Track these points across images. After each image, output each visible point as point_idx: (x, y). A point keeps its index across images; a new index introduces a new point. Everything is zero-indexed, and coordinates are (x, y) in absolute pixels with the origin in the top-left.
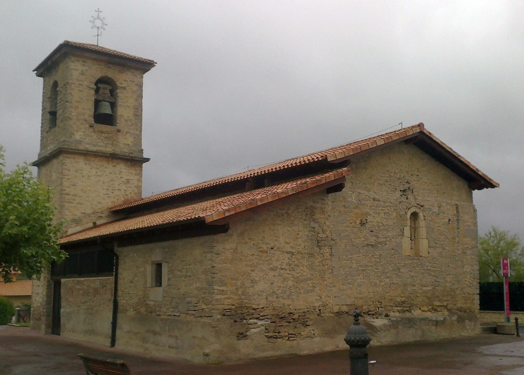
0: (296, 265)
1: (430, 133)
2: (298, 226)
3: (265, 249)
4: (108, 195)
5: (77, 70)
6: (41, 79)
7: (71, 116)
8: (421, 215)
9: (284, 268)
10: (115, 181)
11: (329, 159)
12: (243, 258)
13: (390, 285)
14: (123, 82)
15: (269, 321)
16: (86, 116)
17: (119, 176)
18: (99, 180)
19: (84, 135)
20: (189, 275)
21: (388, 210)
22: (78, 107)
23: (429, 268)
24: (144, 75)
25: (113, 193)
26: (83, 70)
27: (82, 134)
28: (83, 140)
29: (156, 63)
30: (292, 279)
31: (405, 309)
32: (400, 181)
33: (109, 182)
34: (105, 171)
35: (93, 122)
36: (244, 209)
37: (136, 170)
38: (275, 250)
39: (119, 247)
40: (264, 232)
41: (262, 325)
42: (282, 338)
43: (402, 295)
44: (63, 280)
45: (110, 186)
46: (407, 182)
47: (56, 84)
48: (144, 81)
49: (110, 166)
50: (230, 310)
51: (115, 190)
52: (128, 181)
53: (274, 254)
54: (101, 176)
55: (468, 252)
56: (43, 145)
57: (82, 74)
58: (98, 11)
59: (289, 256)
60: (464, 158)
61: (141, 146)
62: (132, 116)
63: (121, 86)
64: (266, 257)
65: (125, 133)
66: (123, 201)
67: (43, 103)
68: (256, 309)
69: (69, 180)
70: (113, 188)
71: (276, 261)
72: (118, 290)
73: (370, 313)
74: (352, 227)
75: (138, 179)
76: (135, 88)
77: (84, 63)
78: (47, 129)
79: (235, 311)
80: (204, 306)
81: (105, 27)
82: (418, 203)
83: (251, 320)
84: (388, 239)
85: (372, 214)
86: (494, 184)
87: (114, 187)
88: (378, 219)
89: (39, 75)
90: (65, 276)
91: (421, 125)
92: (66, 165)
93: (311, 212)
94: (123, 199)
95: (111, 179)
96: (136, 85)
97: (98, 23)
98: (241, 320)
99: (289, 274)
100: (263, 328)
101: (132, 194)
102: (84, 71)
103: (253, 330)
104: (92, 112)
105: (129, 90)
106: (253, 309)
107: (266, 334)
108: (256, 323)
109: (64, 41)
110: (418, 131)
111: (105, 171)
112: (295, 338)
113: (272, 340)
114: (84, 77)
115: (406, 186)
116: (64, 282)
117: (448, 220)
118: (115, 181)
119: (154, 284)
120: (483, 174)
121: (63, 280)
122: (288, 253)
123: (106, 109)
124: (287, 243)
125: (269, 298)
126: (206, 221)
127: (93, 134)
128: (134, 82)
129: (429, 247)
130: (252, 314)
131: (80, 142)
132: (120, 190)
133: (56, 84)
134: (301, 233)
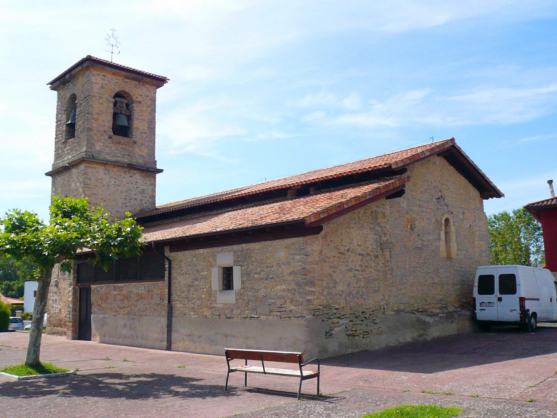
0: (366, 266)
1: (459, 147)
2: (366, 230)
3: (343, 251)
4: (126, 204)
5: (98, 83)
6: (55, 93)
7: (92, 128)
8: (451, 220)
9: (357, 269)
10: (132, 190)
11: (393, 167)
12: (326, 259)
13: (433, 284)
14: (138, 96)
15: (348, 320)
16: (106, 128)
17: (135, 186)
18: (118, 190)
19: (103, 146)
20: (271, 277)
21: (429, 215)
22: (98, 119)
23: (458, 268)
24: (157, 90)
25: (130, 202)
26: (102, 84)
27: (102, 144)
28: (102, 151)
29: (169, 80)
30: (364, 280)
31: (443, 306)
32: (435, 189)
33: (126, 192)
34: (122, 181)
35: (112, 134)
36: (334, 212)
37: (151, 181)
38: (351, 252)
39: (170, 252)
40: (342, 234)
41: (343, 324)
42: (358, 336)
43: (441, 293)
44: (93, 287)
45: (127, 196)
46: (440, 191)
47: (73, 97)
48: (157, 97)
49: (127, 176)
50: (318, 311)
51: (131, 199)
52: (143, 191)
53: (350, 256)
54: (119, 186)
55: (483, 255)
56: (58, 156)
57: (102, 87)
58: (113, 30)
59: (361, 257)
60: (481, 171)
61: (155, 158)
62: (146, 128)
63: (137, 100)
64: (344, 259)
65: (140, 145)
66: (139, 210)
67: (57, 115)
68: (338, 308)
69: (90, 189)
70: (130, 198)
71: (351, 263)
72: (173, 294)
73: (419, 310)
74: (406, 231)
75: (152, 189)
76: (149, 103)
77: (104, 78)
78: (63, 140)
79: (323, 311)
80: (292, 307)
81: (118, 45)
82: (449, 210)
83: (335, 320)
84: (430, 242)
85: (419, 219)
86: (501, 194)
87: (130, 197)
88: (423, 224)
89: (53, 89)
90: (95, 282)
91: (453, 140)
92: (88, 175)
93: (375, 216)
94: (139, 208)
95: (128, 189)
96: (150, 100)
97: (113, 41)
98: (327, 320)
99: (361, 275)
100: (344, 326)
101: (147, 204)
102: (104, 85)
103: (336, 329)
104: (111, 124)
105: (144, 104)
106: (336, 309)
107: (347, 333)
108: (339, 322)
109: (87, 56)
110: (451, 144)
111: (122, 181)
112: (368, 336)
113: (351, 338)
114: (104, 90)
115: (440, 194)
116: (95, 289)
117: (469, 226)
118: (132, 190)
119: (221, 288)
120: (494, 185)
121: (93, 287)
122: (360, 254)
123: (123, 121)
124: (360, 246)
125: (347, 298)
126: (306, 222)
127: (111, 145)
128: (148, 96)
129: (458, 250)
130: (335, 314)
131: (100, 152)
132: (136, 199)
133: (73, 97)
134: (369, 236)
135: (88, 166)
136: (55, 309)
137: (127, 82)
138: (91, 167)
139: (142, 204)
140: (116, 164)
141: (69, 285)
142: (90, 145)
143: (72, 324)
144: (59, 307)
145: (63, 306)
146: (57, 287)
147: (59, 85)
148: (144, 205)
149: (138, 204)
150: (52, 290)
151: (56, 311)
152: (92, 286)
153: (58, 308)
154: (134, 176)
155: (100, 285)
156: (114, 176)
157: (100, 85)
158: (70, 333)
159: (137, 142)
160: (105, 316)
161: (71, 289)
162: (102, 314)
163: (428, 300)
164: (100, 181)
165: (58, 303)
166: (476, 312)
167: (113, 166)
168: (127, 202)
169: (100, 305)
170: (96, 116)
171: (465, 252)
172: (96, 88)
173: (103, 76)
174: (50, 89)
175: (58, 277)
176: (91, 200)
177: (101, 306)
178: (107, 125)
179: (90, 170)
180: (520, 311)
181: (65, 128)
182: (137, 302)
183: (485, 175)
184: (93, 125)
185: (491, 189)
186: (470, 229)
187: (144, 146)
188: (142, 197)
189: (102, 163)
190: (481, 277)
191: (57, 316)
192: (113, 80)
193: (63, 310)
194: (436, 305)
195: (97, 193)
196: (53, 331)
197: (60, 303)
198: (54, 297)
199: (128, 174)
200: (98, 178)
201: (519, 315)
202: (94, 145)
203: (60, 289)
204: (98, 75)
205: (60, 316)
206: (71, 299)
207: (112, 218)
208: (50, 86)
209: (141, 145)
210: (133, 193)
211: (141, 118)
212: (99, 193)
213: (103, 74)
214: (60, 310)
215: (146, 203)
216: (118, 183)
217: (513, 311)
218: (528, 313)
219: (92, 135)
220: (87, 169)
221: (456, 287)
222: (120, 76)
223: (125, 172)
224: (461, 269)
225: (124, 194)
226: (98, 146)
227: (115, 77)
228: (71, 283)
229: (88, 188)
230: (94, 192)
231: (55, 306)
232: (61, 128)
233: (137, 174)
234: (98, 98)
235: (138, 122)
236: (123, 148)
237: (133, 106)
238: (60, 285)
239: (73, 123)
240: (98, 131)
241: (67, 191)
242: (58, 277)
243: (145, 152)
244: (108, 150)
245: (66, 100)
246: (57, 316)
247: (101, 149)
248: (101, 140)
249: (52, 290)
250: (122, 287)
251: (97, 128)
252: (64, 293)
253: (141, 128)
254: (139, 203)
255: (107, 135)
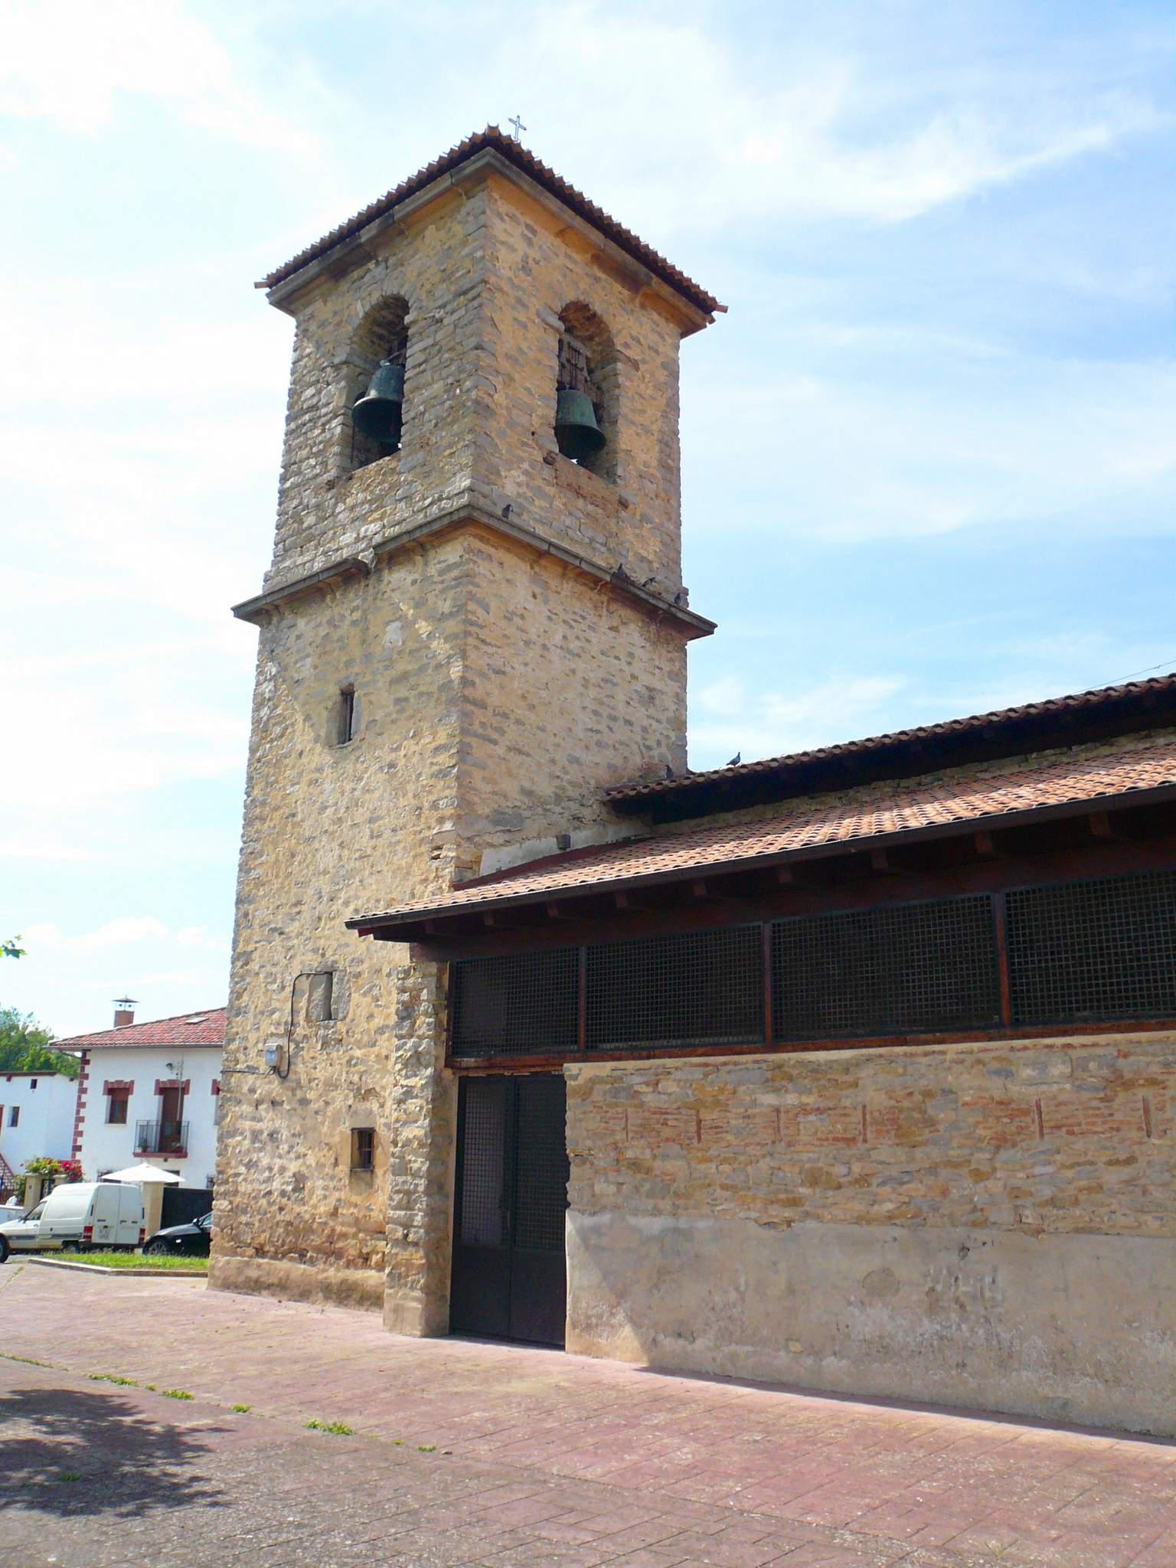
7: (492, 406)
18: (573, 671)
25: (611, 729)
57: (525, 268)
75: (677, 694)
76: (662, 376)
89: (284, 303)
90: (591, 1052)
92: (478, 586)
94: (637, 760)
102: (530, 261)
121: (578, 1073)
127: (551, 491)
135: (480, 551)
136: (267, 1174)
137: (597, 279)
138: (490, 558)
139: (649, 748)
140: (577, 563)
141: (405, 1065)
142: (485, 471)
143: (427, 1256)
144: (293, 1167)
145: (320, 1166)
146: (284, 1078)
147: (317, 276)
148: (655, 753)
149: (636, 743)
150: (252, 1091)
151: (276, 1185)
152: (571, 1068)
153: (283, 1170)
154: (623, 629)
155: (640, 1064)
156: (563, 616)
157: (517, 257)
158: (413, 1302)
159: (631, 506)
160: (683, 1223)
161: (417, 1082)
162: (657, 1212)
164: (517, 620)
165: (285, 1147)
167: (560, 570)
168: (602, 727)
169: (635, 1165)
170: (505, 365)
172: (506, 262)
173: (527, 226)
174: (267, 300)
175: (290, 1034)
176: (488, 694)
177: (649, 1171)
178: (540, 412)
179: (483, 568)
181: (339, 430)
182: (998, 1148)
184: (496, 396)
187: (649, 526)
188: (649, 717)
189: (528, 547)
191: (281, 1209)
192: (557, 256)
193: (320, 1183)
195: (508, 669)
196: (253, 1273)
197: (301, 1150)
198: (260, 1120)
199: (604, 618)
200: (511, 608)
202: (498, 473)
203: (299, 1085)
204: (512, 218)
205: (297, 1209)
206: (420, 1133)
207: (557, 782)
208: (267, 290)
209: (641, 521)
210: (621, 697)
211: (638, 419)
212: (513, 668)
213: (529, 222)
214: (299, 1181)
215: (659, 743)
216: (574, 645)
219: (493, 435)
220: (475, 562)
222: (585, 245)
223: (596, 607)
225: (593, 692)
226: (512, 484)
227: (563, 247)
228: (417, 1055)
229: (478, 638)
230: (498, 663)
231: (265, 1162)
232: (317, 432)
233: (632, 626)
234: (513, 301)
235: (631, 430)
236: (588, 515)
237: (615, 369)
238: (300, 1068)
239: (392, 397)
240: (511, 424)
241: (349, 664)
242: (290, 1034)
243: (651, 549)
244: (541, 508)
245: (348, 329)
246: (281, 1209)
247: (519, 495)
248: (521, 460)
249: (252, 1091)
250: (847, 1067)
251: (508, 408)
252: (327, 1103)
253: (642, 457)
254: (638, 738)
255: (541, 448)
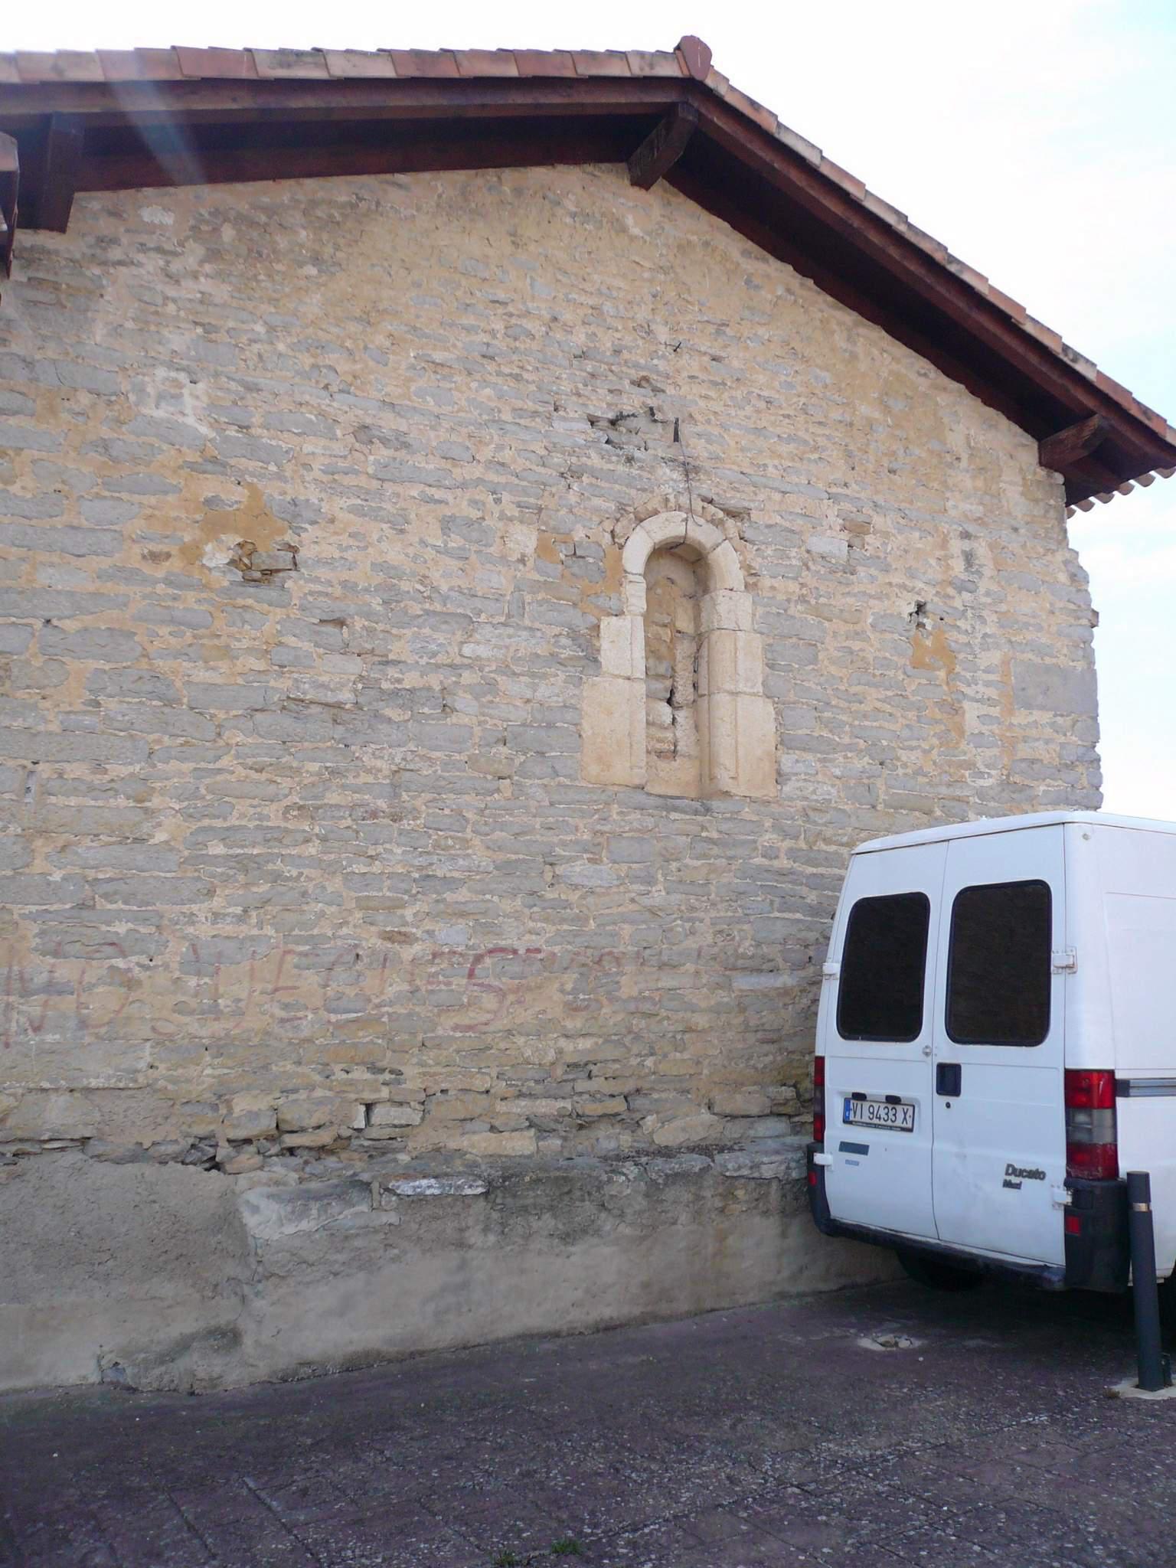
23: (784, 863)
163: (409, 1071)
166: (819, 1159)
171: (862, 763)
180: (1068, 1184)
183: (1022, 309)
185: (1089, 402)
186: (920, 625)
190: (868, 912)
194: (501, 1107)
201: (1058, 1220)
217: (1027, 1183)
218: (1143, 1207)
221: (744, 983)
224: (811, 870)
